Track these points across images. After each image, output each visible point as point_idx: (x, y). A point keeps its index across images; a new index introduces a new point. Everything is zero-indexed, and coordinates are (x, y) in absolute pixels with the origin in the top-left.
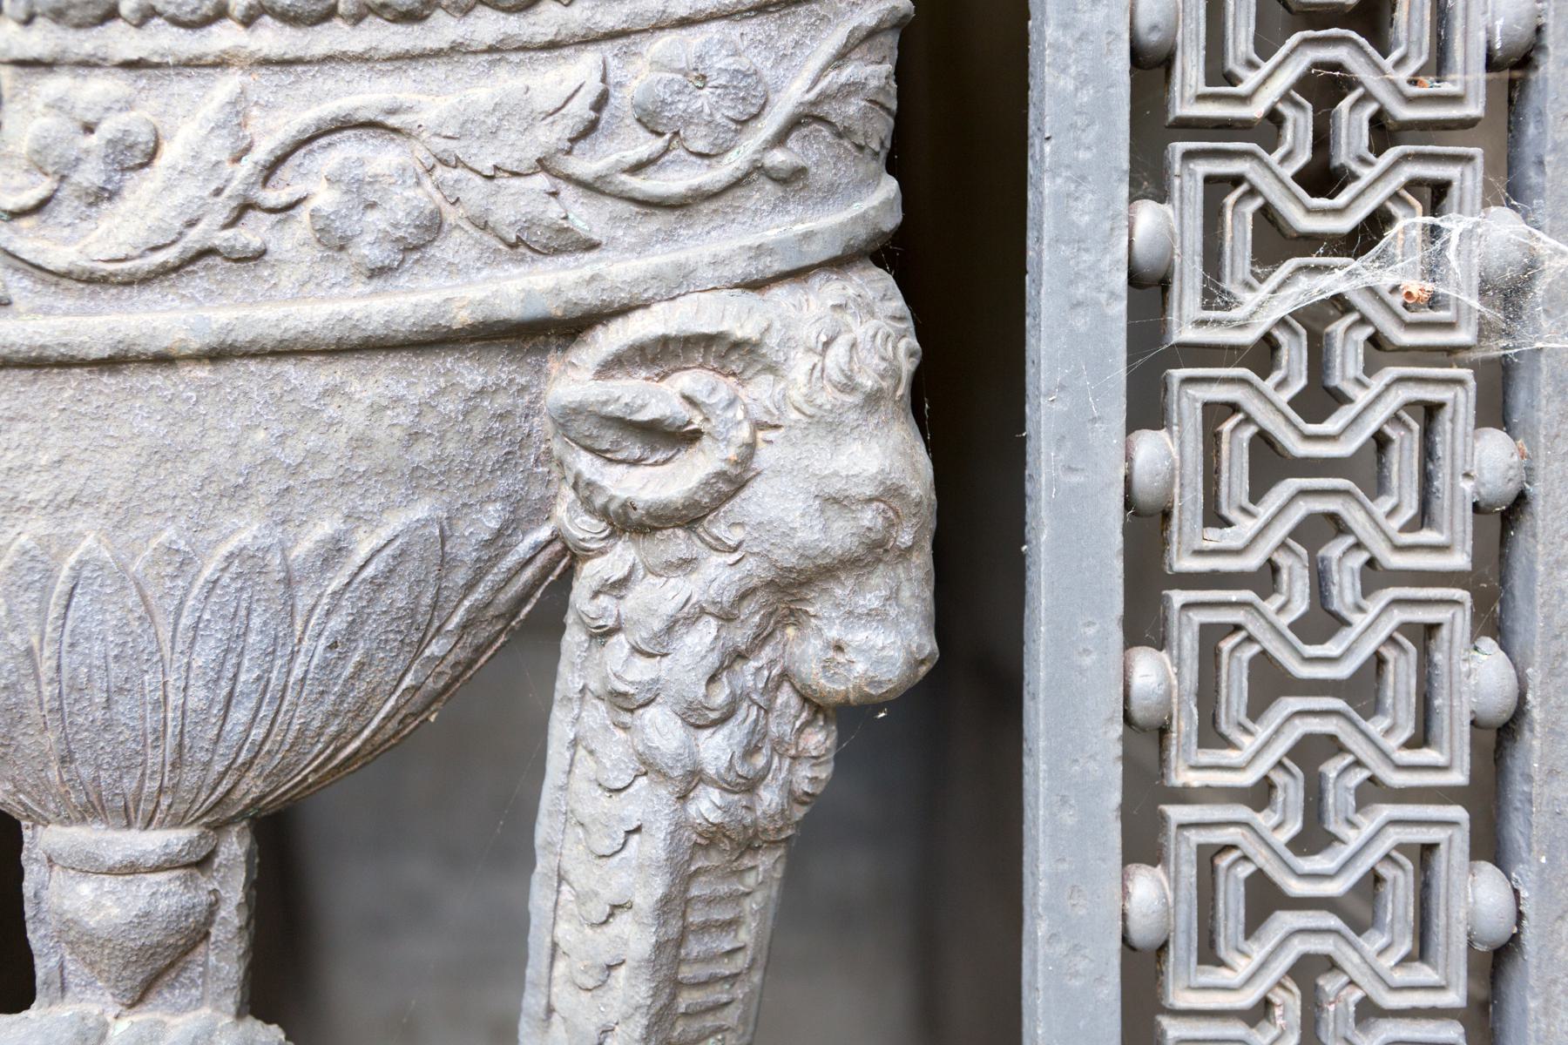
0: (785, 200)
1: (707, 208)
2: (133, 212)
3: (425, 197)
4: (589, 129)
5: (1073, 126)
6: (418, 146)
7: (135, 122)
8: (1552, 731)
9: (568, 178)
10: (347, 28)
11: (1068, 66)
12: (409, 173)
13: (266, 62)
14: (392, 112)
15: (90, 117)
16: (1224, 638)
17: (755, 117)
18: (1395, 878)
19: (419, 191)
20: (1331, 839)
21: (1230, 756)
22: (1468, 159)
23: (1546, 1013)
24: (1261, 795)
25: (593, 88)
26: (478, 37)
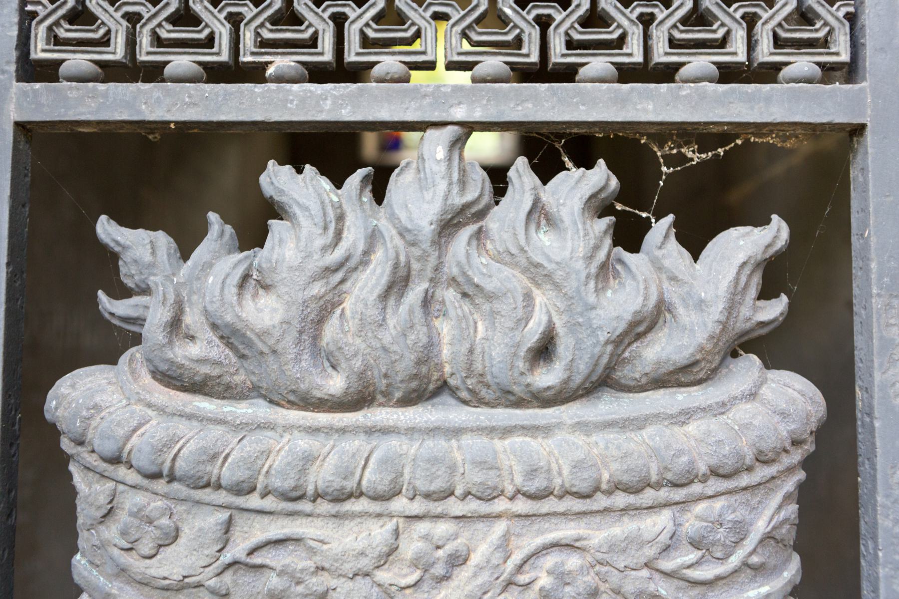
0: (755, 576)
1: (721, 583)
2: (458, 587)
3: (590, 579)
4: (667, 548)
5: (893, 544)
6: (588, 555)
7: (458, 544)
9: (657, 570)
10: (556, 500)
11: (888, 515)
12: (585, 568)
13: (520, 516)
14: (577, 540)
15: (440, 543)
17: (742, 539)
19: (589, 577)
25: (670, 527)
26: (616, 504)
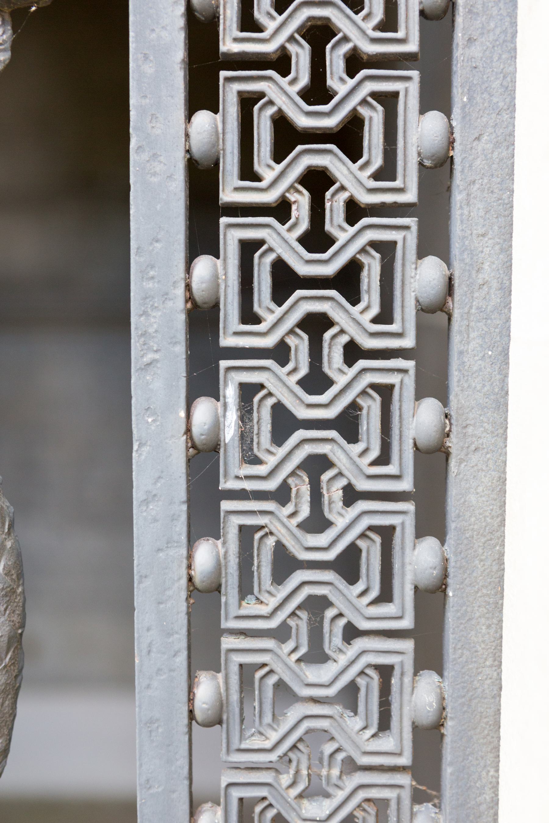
8: (470, 12)
16: (256, 670)
18: (371, 118)
20: (327, 524)
21: (262, 470)
22: (407, 228)
23: (468, 204)
24: (282, 495)
